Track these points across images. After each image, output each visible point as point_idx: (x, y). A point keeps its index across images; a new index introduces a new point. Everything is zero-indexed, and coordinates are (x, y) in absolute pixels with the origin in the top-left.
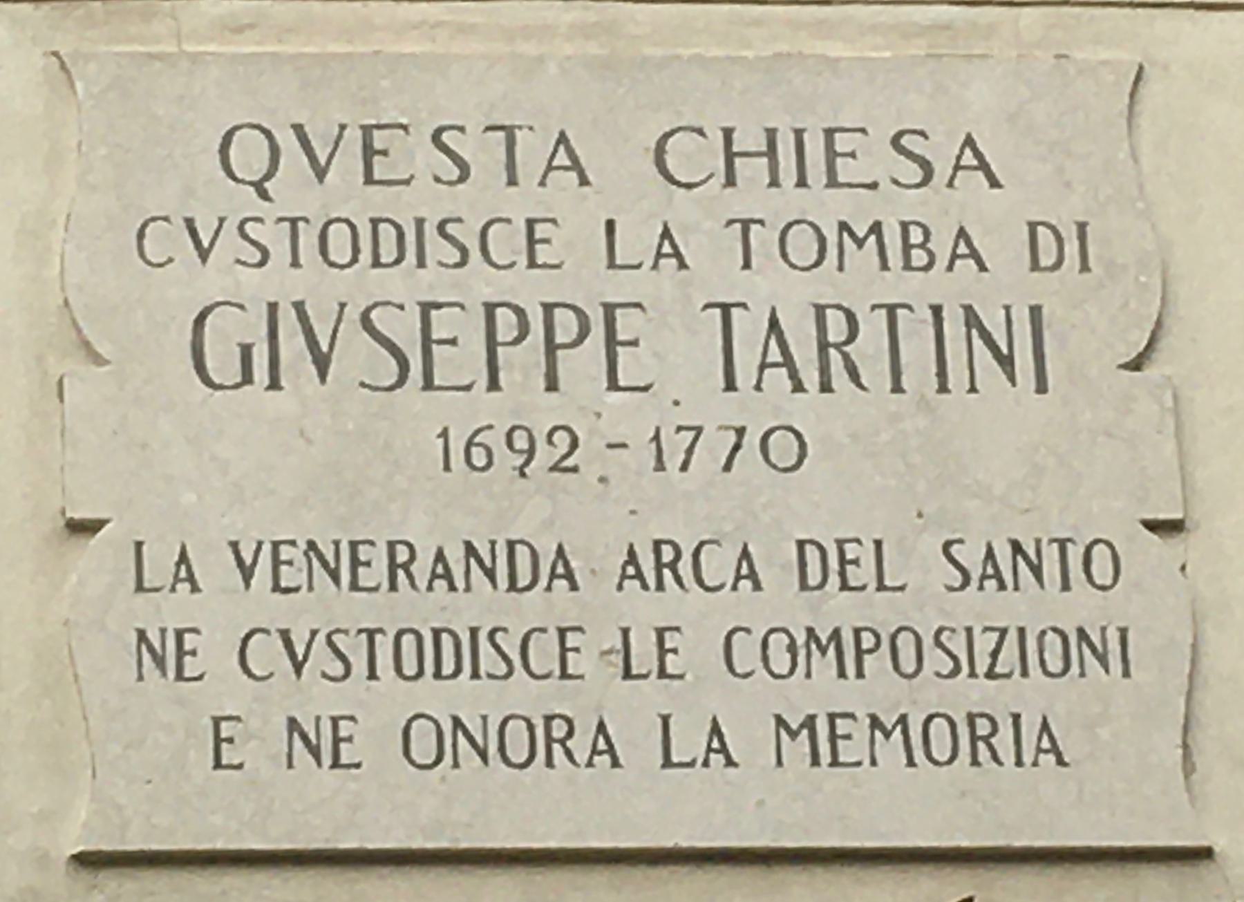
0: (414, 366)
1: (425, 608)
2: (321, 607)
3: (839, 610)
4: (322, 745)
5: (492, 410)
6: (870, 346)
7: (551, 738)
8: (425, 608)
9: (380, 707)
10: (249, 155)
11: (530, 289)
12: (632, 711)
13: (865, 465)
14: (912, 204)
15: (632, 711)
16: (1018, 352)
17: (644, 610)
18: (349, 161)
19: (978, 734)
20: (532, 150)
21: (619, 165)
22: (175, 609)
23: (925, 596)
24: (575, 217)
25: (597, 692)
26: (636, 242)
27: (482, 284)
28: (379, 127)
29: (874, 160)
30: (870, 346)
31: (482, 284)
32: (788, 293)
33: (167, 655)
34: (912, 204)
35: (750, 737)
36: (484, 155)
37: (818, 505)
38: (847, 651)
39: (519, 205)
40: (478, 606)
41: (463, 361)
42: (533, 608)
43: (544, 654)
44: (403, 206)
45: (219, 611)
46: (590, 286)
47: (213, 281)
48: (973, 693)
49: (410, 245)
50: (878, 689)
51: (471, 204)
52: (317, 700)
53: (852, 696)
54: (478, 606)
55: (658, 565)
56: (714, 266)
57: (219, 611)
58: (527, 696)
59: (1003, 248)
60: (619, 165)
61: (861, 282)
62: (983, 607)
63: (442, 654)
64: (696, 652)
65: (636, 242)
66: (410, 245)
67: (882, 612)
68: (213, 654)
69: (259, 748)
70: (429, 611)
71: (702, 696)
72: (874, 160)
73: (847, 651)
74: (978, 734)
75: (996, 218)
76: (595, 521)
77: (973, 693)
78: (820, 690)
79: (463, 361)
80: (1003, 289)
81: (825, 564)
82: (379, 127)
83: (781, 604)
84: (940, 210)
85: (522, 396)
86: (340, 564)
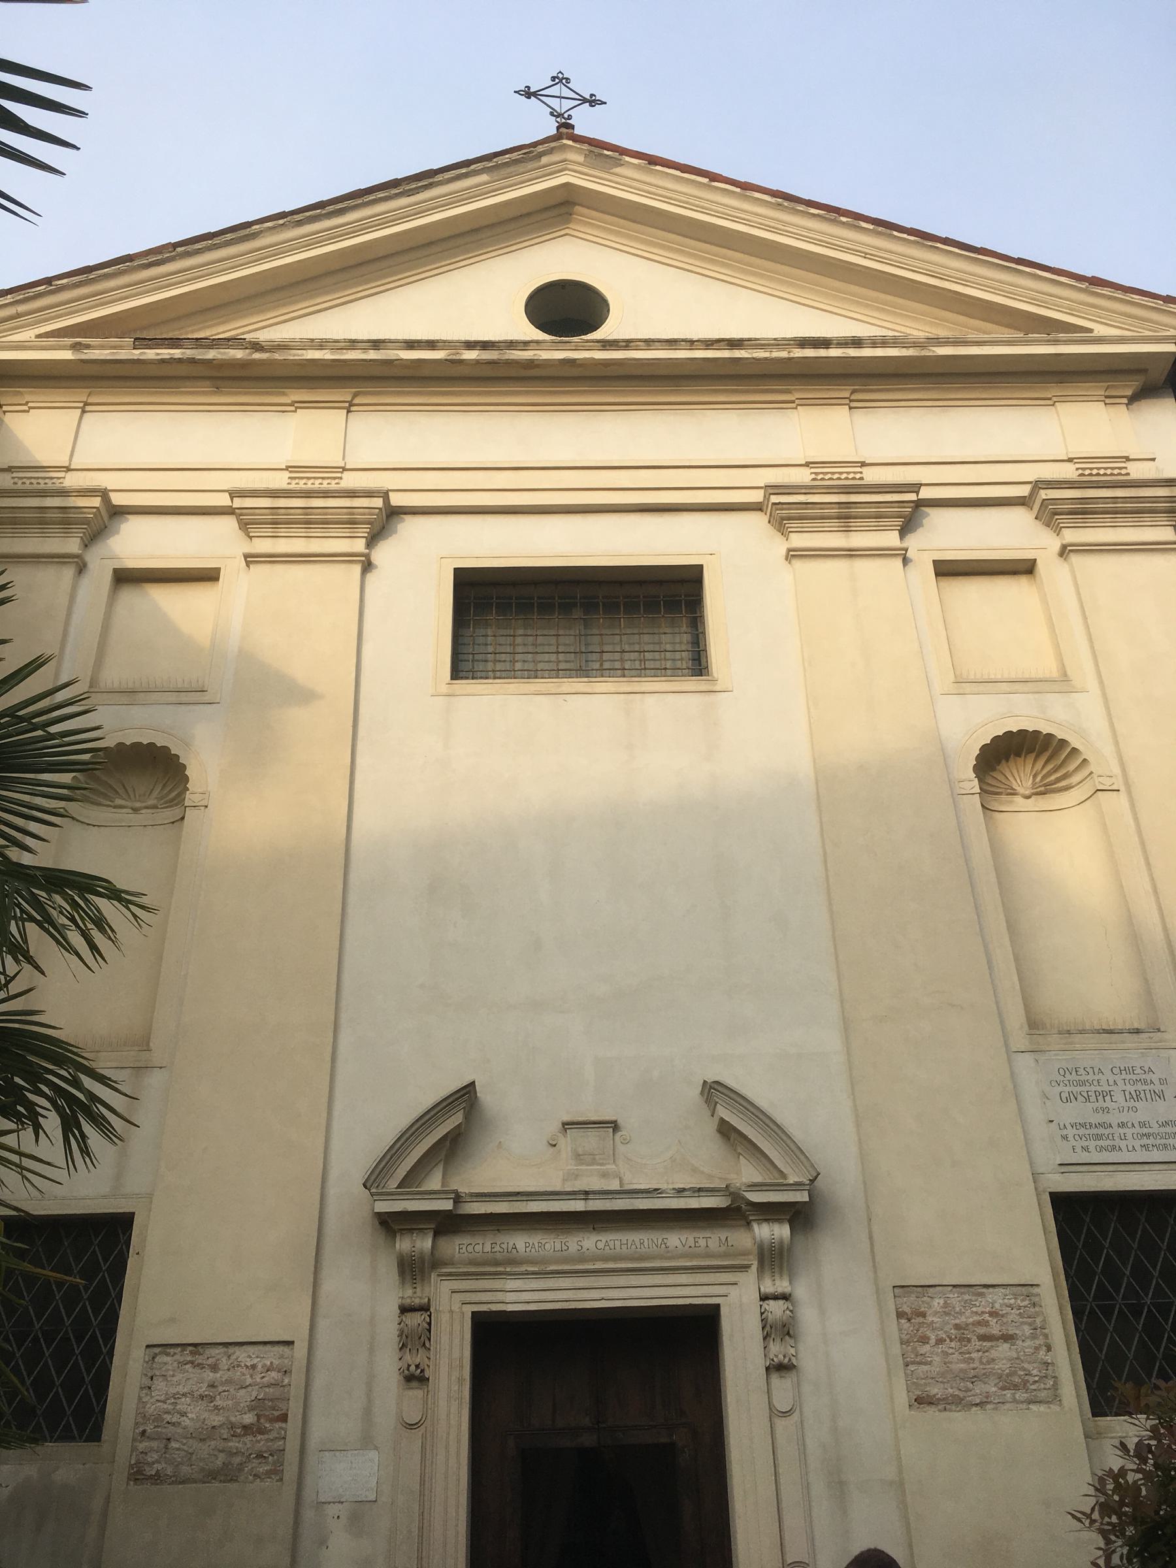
0: (1088, 1099)
1: (1095, 1131)
2: (1082, 1131)
3: (1145, 1131)
4: (1086, 1149)
5: (1097, 1104)
6: (1142, 1095)
7: (1114, 1148)
8: (1095, 1131)
9: (1092, 1144)
10: (1062, 1071)
11: (1099, 1089)
12: (1123, 1144)
13: (1146, 1111)
14: (1144, 1076)
15: (1123, 1144)
16: (1161, 1096)
17: (1122, 1131)
18: (1074, 1073)
19: (1165, 1146)
20: (1096, 1071)
21: (1107, 1072)
22: (1065, 1132)
23: (1155, 1129)
24: (1103, 1078)
25: (1118, 1142)
26: (1111, 1083)
27: (1093, 1088)
28: (1006, 1045)
29: (1138, 1071)
30: (1142, 1095)
31: (1093, 1088)
32: (1132, 1089)
33: (1065, 1138)
34: (1144, 1076)
35: (1138, 1148)
36: (1091, 1071)
37: (1141, 1116)
38: (1147, 1136)
39: (1096, 1078)
40: (1101, 1131)
41: (1093, 1099)
42: (1106, 1132)
43: (1095, 1083)
44: (1081, 1078)
45: (1070, 1132)
46: (1107, 1088)
47: (1060, 1089)
48: (1164, 1141)
49: (1083, 1083)
50: (1151, 1141)
51: (1090, 1077)
52: (1085, 1144)
53: (1148, 1142)
54: (1101, 1131)
55: (1122, 1125)
56: (1121, 1086)
57: (1070, 1132)
58: (1108, 1142)
59: (1157, 1082)
60: (1107, 1072)
61: (1140, 1087)
62: (1162, 1130)
63: (1099, 1137)
64: (1129, 1136)
65: (1111, 1083)
66: (1083, 1083)
67: (1151, 1131)
68: (1070, 1138)
69: (1078, 1149)
70: (1095, 1131)
71: (1131, 1142)
72: (1138, 1071)
73: (1147, 1136)
74: (1165, 1146)
75: (1155, 1078)
76: (1114, 1118)
77: (1164, 1141)
78: (1145, 1141)
79: (1093, 1099)
80: (1157, 1087)
81: (1143, 1124)
82: (1006, 1045)
83: (1137, 1130)
84: (1148, 1077)
85: (1101, 1103)
86: (1083, 1125)
